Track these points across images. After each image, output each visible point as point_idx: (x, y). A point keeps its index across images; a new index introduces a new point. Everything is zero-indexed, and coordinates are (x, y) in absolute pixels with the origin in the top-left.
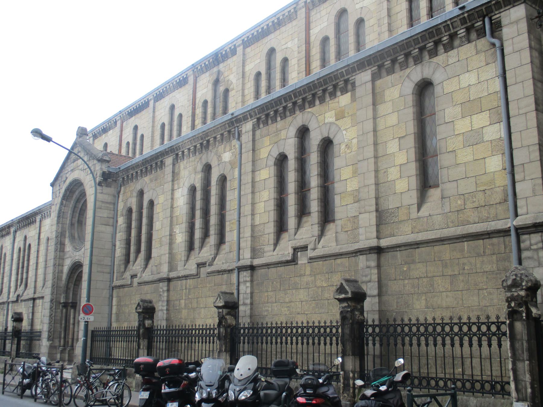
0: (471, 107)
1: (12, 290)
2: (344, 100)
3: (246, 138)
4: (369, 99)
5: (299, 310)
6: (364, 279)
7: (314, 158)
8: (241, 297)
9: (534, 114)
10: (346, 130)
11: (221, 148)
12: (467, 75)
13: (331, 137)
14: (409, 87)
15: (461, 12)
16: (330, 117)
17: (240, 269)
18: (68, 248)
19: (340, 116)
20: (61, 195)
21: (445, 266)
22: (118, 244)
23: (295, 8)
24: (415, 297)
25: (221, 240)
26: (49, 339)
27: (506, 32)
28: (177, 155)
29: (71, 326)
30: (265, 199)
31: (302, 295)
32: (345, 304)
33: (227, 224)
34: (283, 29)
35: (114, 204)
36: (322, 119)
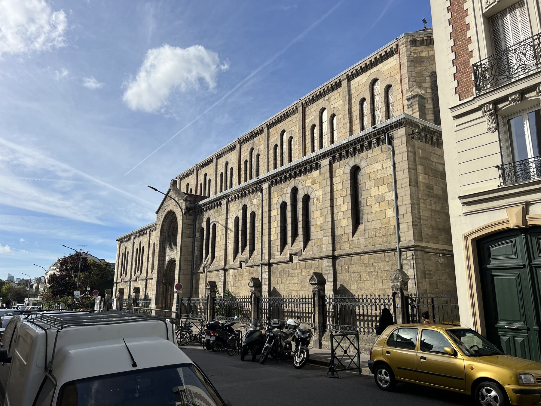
0: (378, 182)
1: (133, 274)
2: (316, 173)
3: (266, 192)
4: (328, 175)
5: (293, 288)
6: (326, 272)
7: (300, 205)
8: (263, 280)
9: (409, 187)
10: (316, 190)
11: (252, 196)
12: (377, 164)
13: (309, 194)
14: (348, 170)
15: (373, 130)
16: (308, 183)
17: (263, 265)
18: (168, 250)
19: (314, 183)
20: (162, 219)
21: (366, 267)
22: (196, 248)
23: (296, 107)
24: (352, 283)
25: (252, 249)
26: (156, 304)
27: (396, 142)
28: (228, 199)
29: (169, 296)
30: (276, 226)
31: (295, 280)
32: (315, 286)
33: (256, 239)
34: (290, 119)
35: (193, 225)
36: (305, 183)
